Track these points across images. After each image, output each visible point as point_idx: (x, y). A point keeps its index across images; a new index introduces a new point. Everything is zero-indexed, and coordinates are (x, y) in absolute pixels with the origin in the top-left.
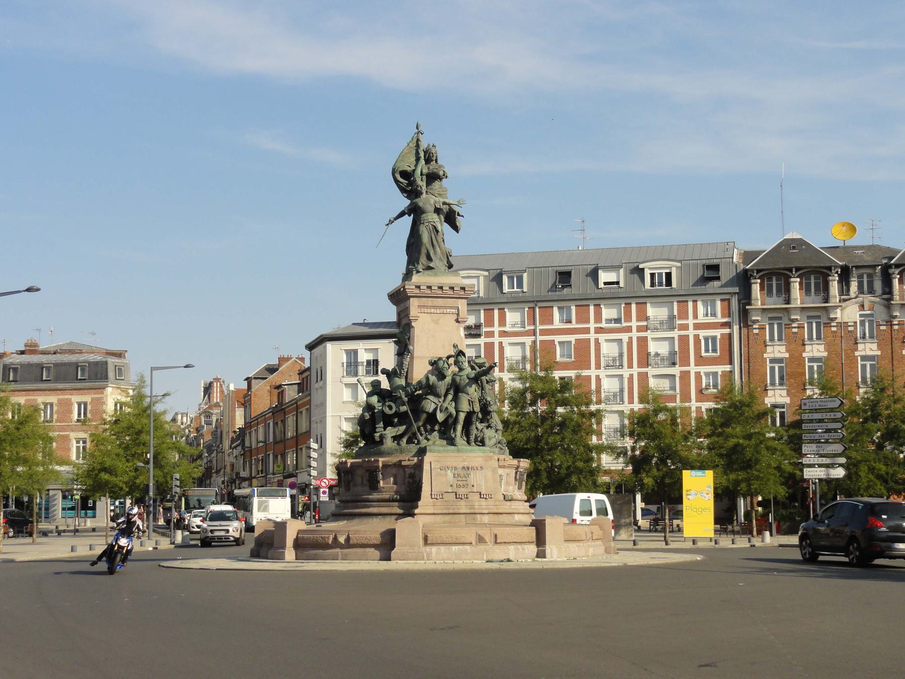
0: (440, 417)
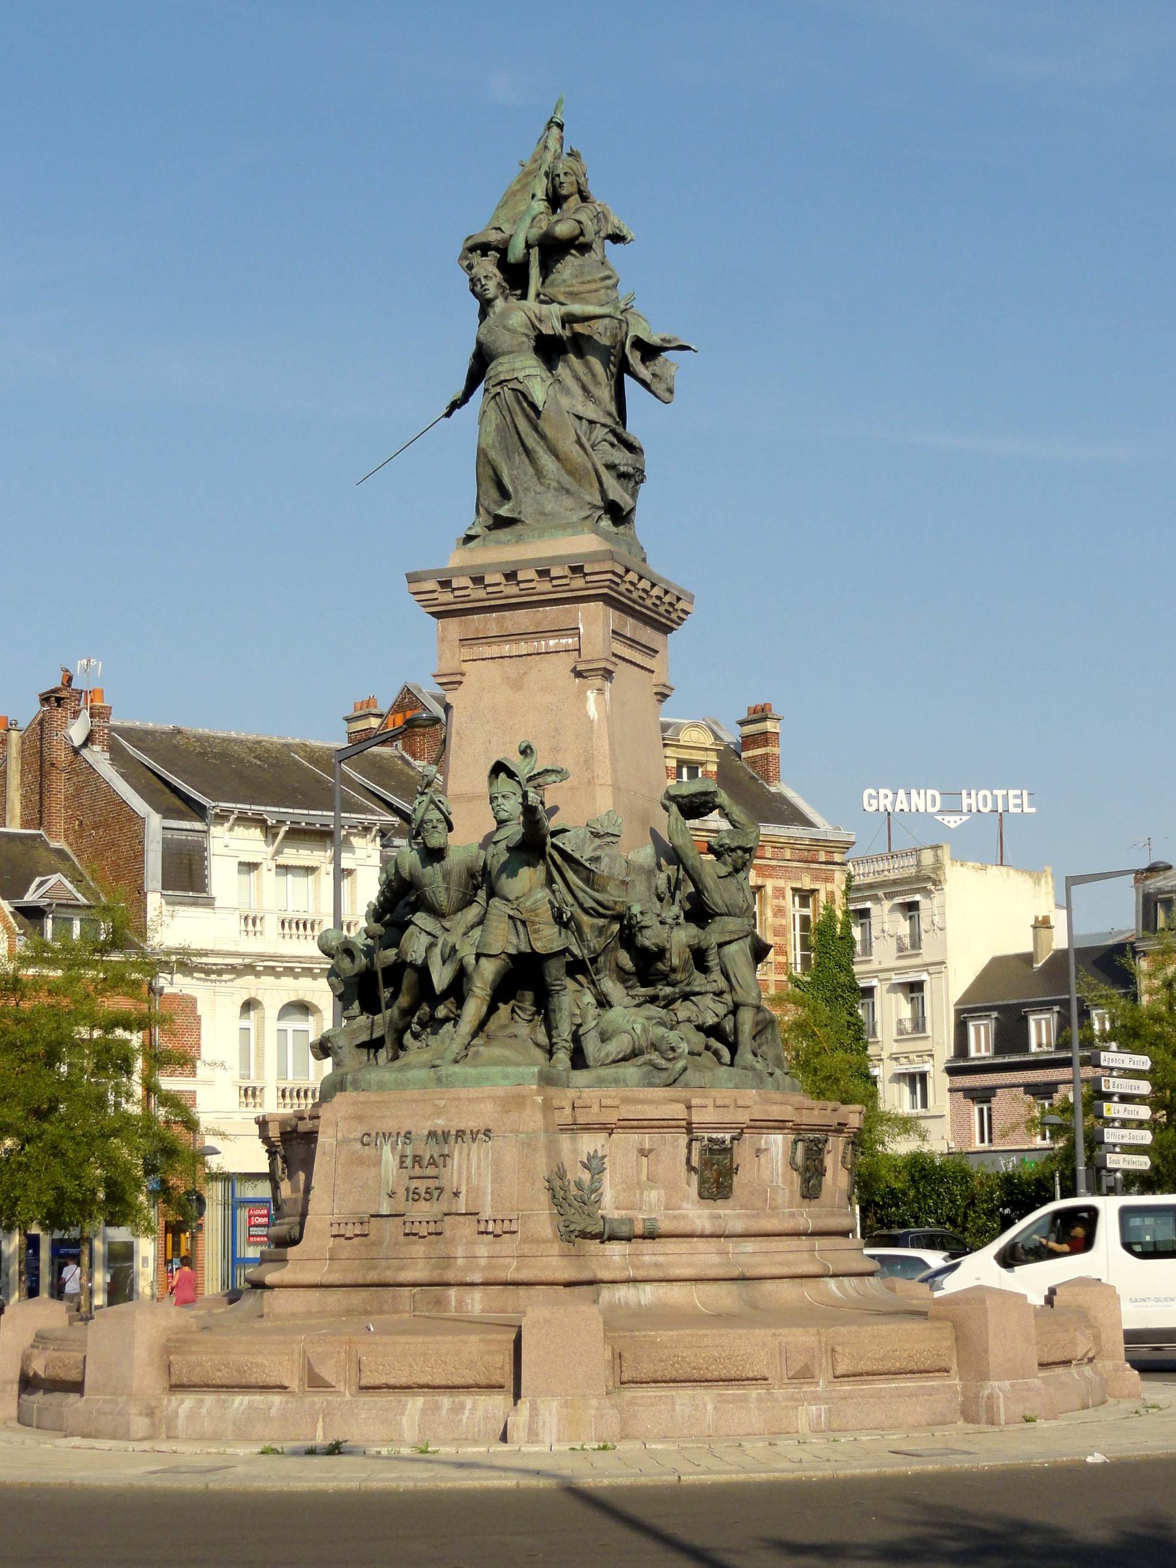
0: (441, 977)
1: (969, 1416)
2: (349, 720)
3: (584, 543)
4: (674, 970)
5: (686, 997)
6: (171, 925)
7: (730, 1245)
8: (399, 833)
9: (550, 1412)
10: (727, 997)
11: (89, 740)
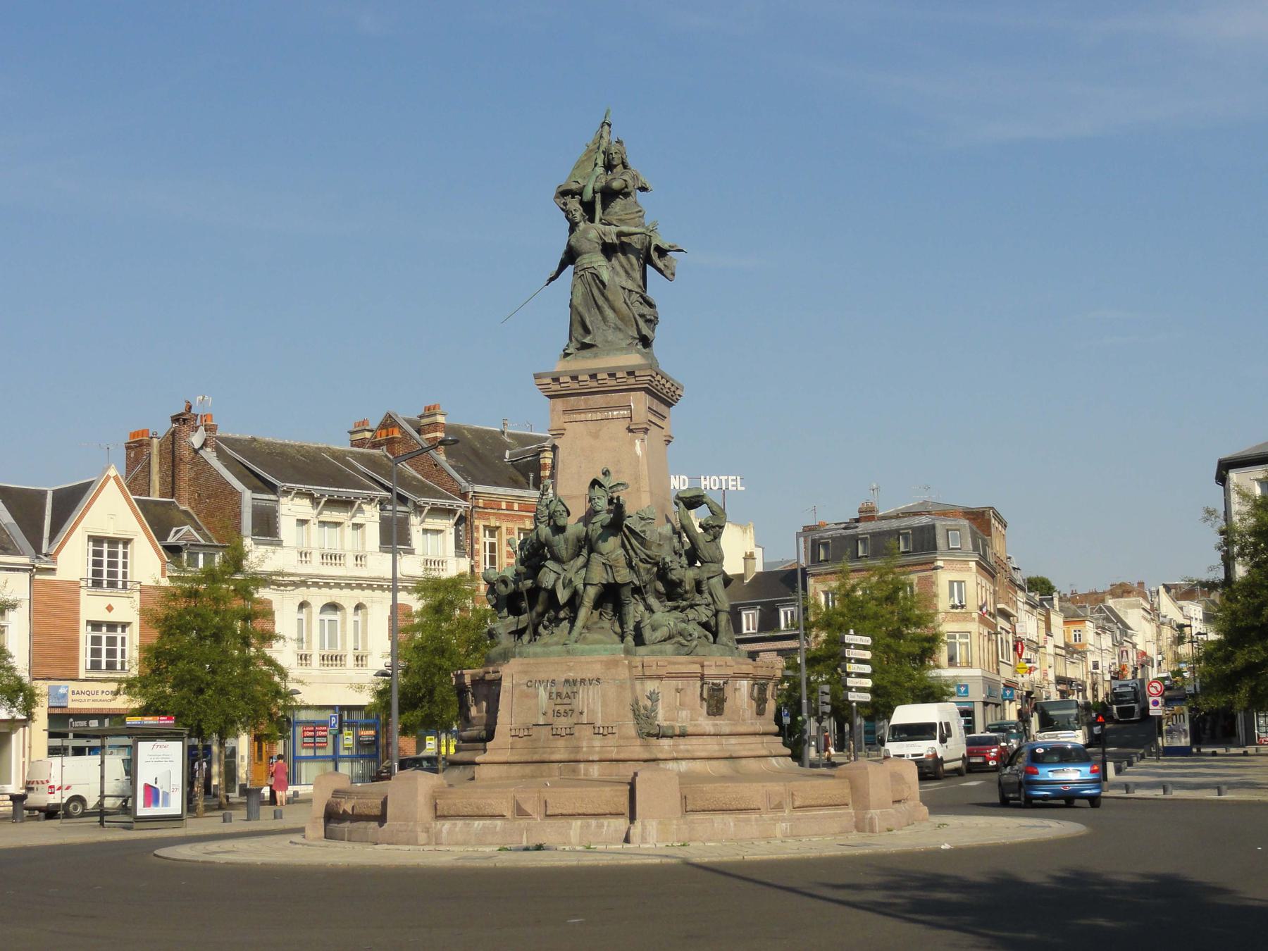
0: (563, 596)
1: (859, 828)
2: (351, 433)
3: (633, 359)
4: (686, 592)
5: (692, 606)
6: (259, 558)
7: (724, 740)
8: (390, 502)
9: (653, 826)
10: (712, 607)
11: (205, 445)
